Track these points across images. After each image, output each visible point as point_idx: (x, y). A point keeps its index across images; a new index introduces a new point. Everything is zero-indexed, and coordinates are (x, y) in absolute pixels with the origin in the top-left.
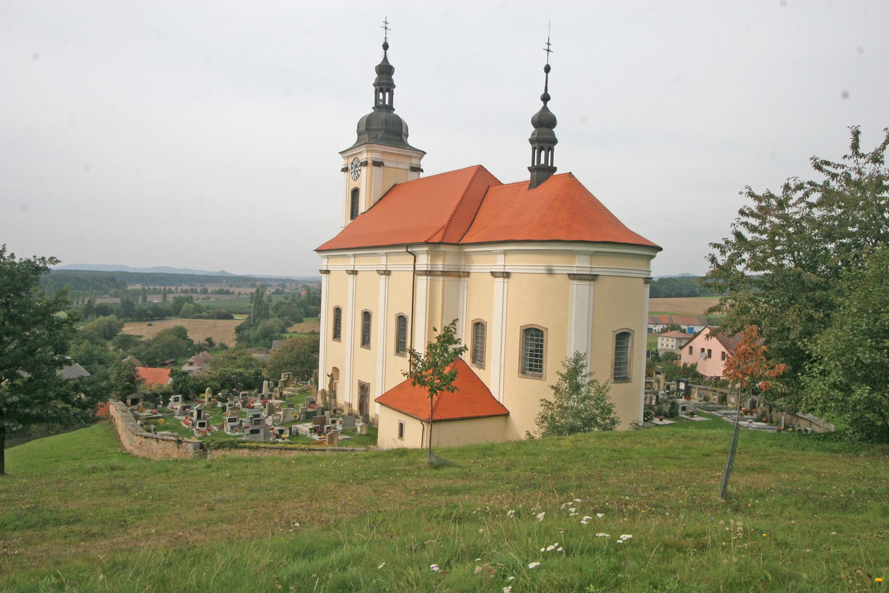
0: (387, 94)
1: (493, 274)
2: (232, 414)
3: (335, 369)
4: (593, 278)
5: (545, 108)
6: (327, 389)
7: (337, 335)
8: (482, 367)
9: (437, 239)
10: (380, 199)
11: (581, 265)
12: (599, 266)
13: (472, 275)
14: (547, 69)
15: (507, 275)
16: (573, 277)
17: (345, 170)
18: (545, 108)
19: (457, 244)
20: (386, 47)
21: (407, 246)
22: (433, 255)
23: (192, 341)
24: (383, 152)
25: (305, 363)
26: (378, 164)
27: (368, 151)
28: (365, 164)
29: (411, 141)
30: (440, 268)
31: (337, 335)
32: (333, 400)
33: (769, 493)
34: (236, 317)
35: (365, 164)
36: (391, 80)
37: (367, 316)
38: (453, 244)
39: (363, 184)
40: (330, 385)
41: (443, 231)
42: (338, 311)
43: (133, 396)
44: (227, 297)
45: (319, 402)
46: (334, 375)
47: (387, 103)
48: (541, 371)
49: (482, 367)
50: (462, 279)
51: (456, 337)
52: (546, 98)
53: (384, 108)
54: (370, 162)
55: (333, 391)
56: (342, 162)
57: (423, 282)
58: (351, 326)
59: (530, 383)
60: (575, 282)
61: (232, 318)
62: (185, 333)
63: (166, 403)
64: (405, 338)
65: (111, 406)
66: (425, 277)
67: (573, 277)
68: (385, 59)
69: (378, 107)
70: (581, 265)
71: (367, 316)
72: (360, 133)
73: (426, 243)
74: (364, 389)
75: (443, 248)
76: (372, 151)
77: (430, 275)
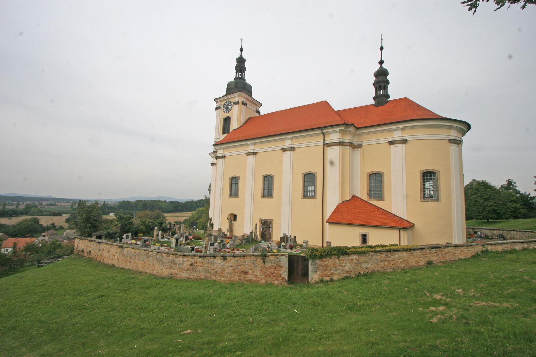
5: (381, 67)
14: (382, 49)
18: (381, 67)
20: (241, 50)
22: (343, 133)
23: (42, 225)
26: (244, 104)
27: (239, 96)
28: (237, 103)
34: (64, 215)
35: (237, 103)
43: (98, 233)
44: (54, 207)
50: (356, 149)
54: (240, 102)
56: (215, 105)
61: (61, 215)
62: (38, 221)
63: (121, 238)
76: (242, 96)
77: (343, 145)
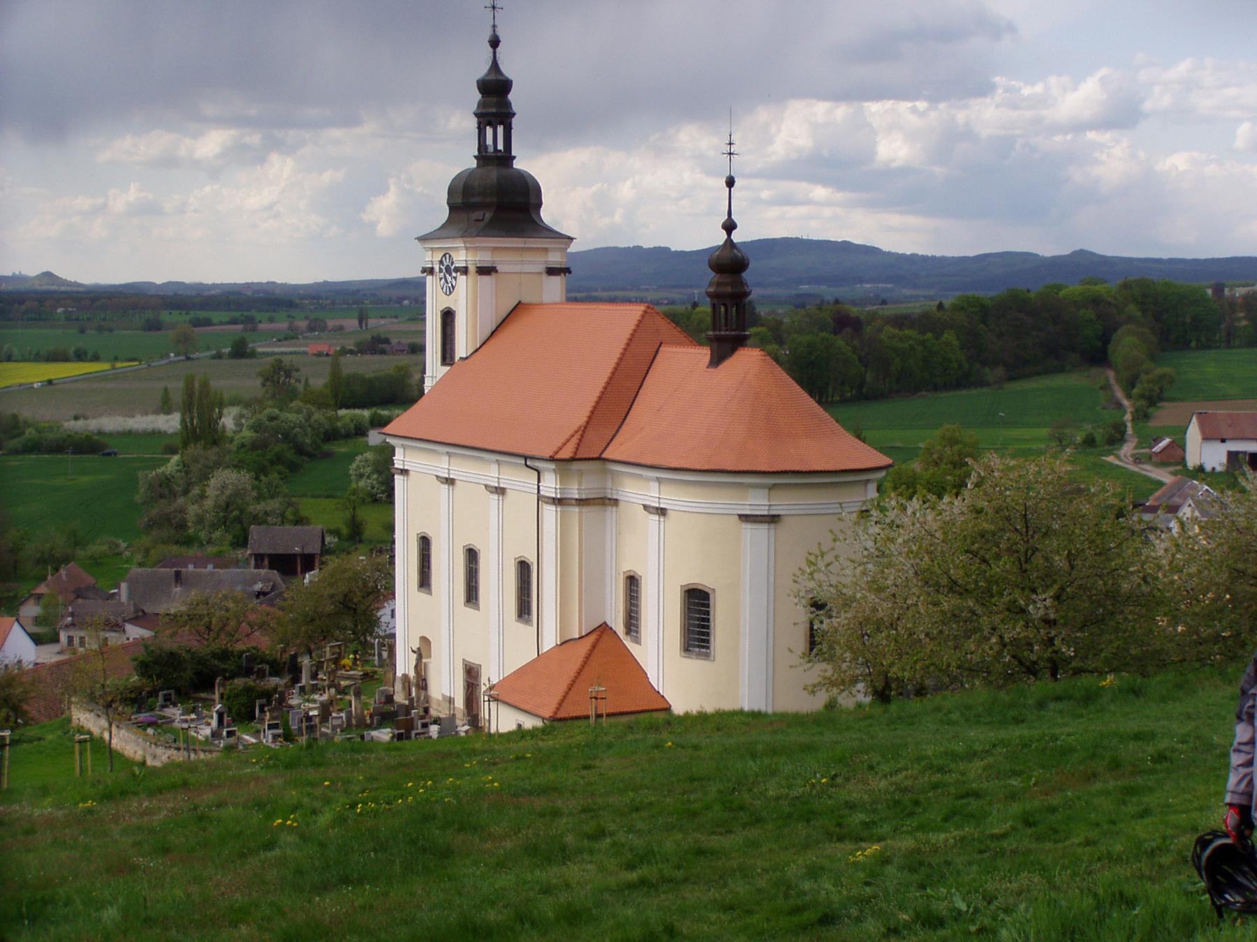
0: (500, 129)
1: (646, 507)
2: (272, 718)
3: (425, 641)
4: (773, 519)
6: (412, 674)
7: (425, 581)
8: (637, 641)
9: (566, 453)
10: (493, 333)
11: (757, 502)
12: (782, 503)
13: (621, 504)
15: (662, 512)
16: (745, 518)
19: (599, 459)
20: (495, 43)
21: (526, 458)
22: (563, 475)
24: (495, 249)
25: (357, 614)
26: (484, 271)
28: (465, 271)
29: (548, 214)
31: (425, 581)
32: (423, 693)
35: (465, 271)
36: (508, 104)
37: (472, 555)
38: (593, 459)
40: (416, 667)
41: (577, 436)
42: (425, 542)
45: (400, 698)
46: (422, 652)
47: (500, 147)
48: (708, 648)
49: (637, 641)
53: (496, 159)
54: (472, 269)
55: (422, 683)
57: (550, 512)
58: (447, 569)
59: (694, 665)
60: (749, 526)
64: (529, 595)
66: (553, 508)
67: (745, 518)
68: (495, 66)
69: (484, 157)
70: (757, 502)
71: (472, 555)
72: (453, 208)
73: (552, 459)
74: (472, 673)
75: (576, 466)
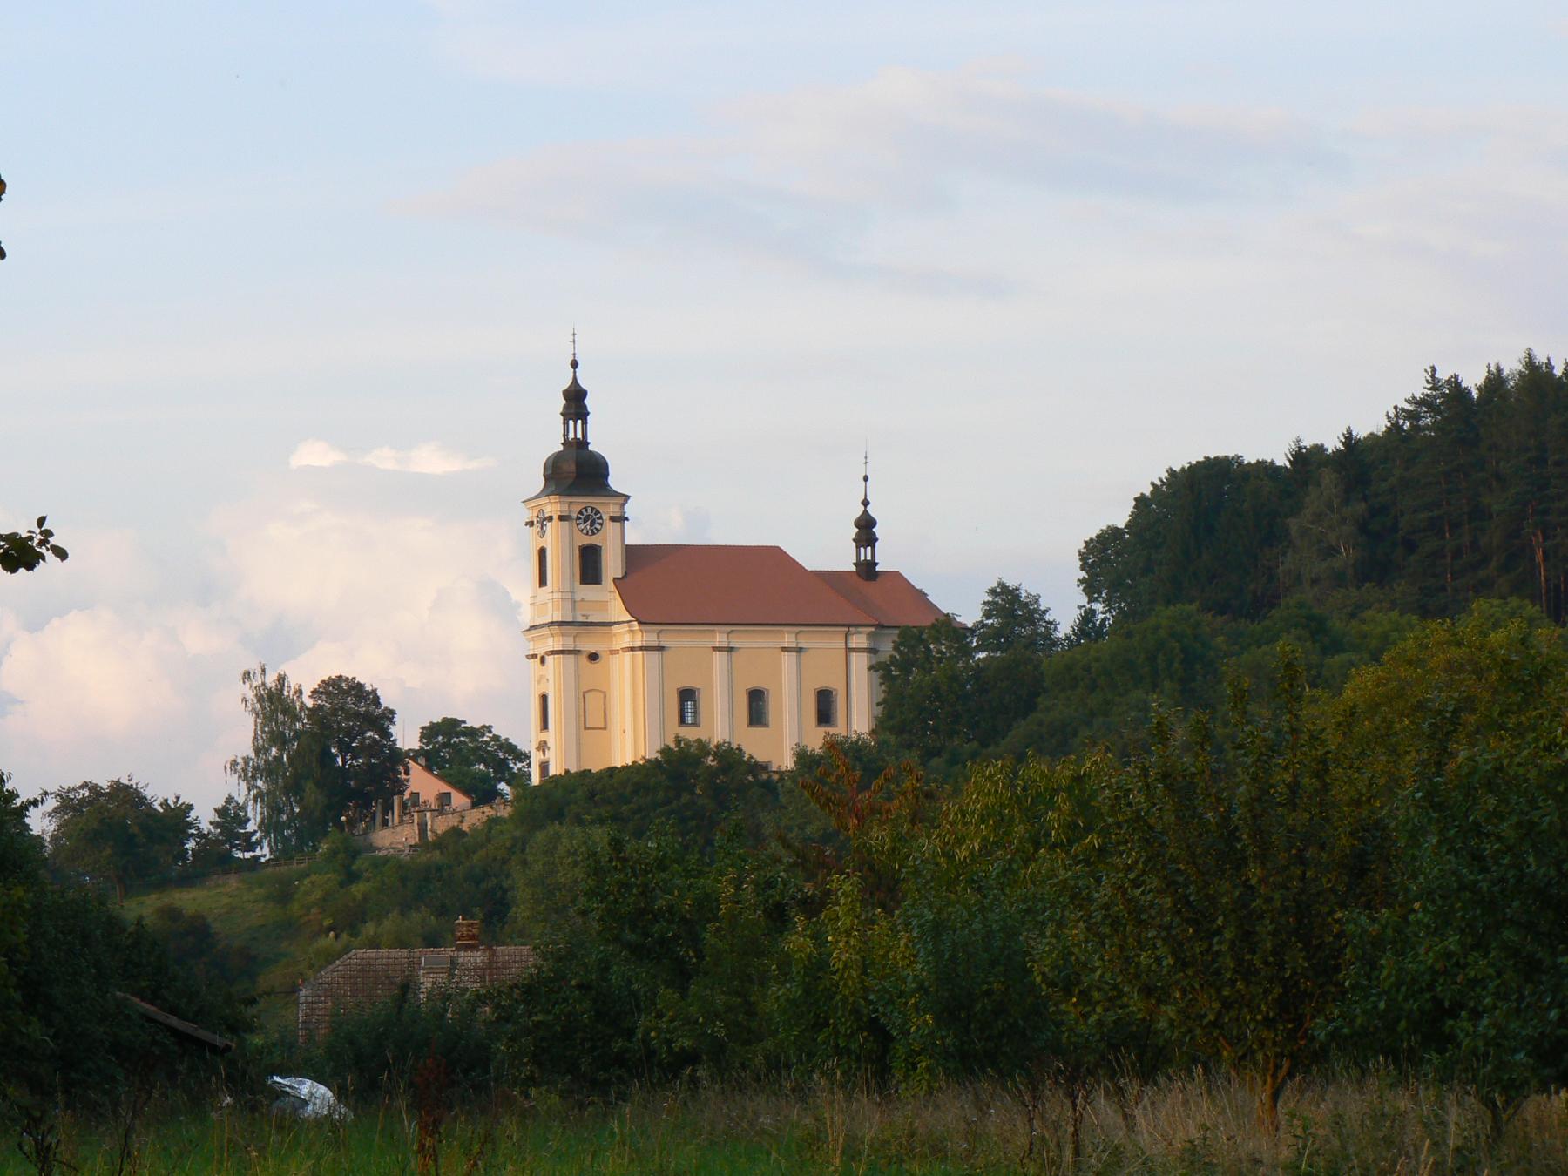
5: (866, 512)
14: (866, 479)
17: (531, 524)
18: (866, 512)
20: (575, 365)
29: (614, 482)
30: (639, 644)
33: (593, 822)
39: (549, 542)
51: (876, 675)
52: (866, 503)
54: (555, 517)
65: (330, 1094)
68: (575, 378)
